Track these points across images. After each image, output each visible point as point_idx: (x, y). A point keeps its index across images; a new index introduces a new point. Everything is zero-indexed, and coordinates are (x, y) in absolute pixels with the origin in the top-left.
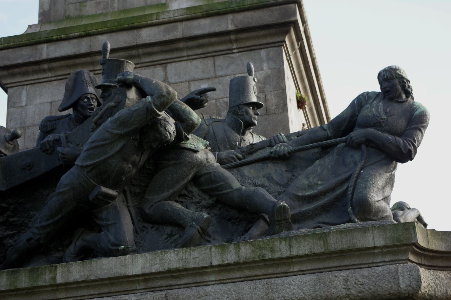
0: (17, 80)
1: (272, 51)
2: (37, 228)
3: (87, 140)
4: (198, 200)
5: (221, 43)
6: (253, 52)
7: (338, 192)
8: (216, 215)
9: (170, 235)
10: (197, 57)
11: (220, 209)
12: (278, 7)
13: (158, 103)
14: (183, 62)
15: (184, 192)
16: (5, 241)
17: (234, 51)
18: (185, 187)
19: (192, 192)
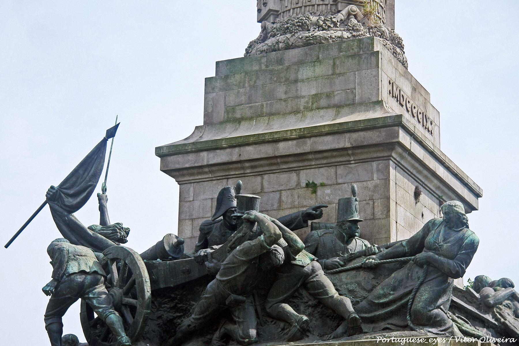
0: (186, 179)
1: (382, 164)
2: (193, 318)
3: (225, 259)
4: (305, 301)
5: (342, 156)
6: (366, 163)
7: (403, 301)
8: (319, 312)
9: (283, 329)
10: (324, 166)
11: (322, 308)
12: (385, 129)
13: (268, 241)
14: (312, 170)
15: (297, 294)
16: (175, 321)
17: (351, 162)
18: (297, 290)
19: (302, 295)
